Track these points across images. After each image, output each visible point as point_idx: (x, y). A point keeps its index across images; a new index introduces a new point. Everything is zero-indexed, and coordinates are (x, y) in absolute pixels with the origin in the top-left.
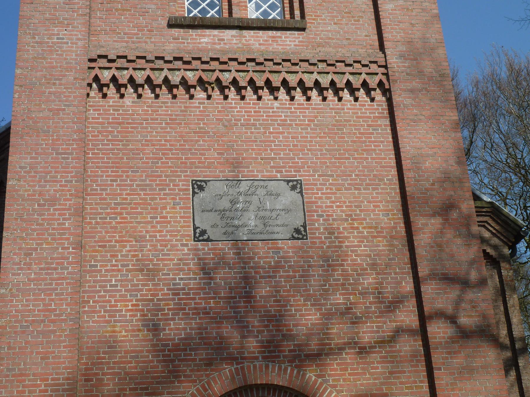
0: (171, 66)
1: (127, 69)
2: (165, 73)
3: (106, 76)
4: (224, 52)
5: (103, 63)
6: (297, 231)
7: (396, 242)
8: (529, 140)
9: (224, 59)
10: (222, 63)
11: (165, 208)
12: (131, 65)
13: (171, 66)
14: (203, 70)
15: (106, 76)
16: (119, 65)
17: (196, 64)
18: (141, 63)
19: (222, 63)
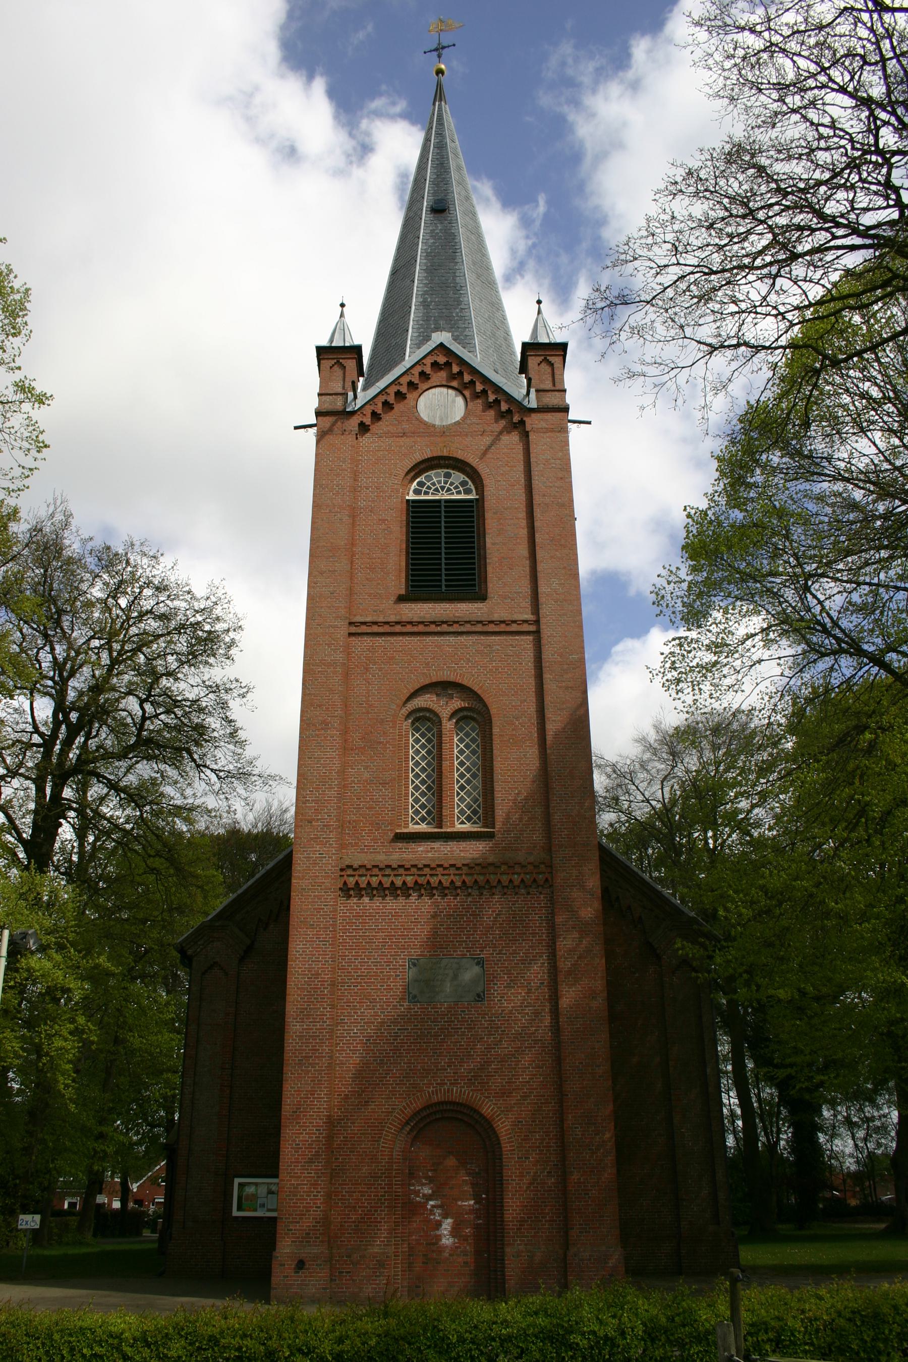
0: (396, 872)
1: (366, 875)
2: (391, 878)
3: (351, 881)
4: (433, 859)
5: (350, 872)
6: (478, 995)
7: (161, 996)
8: (904, 446)
9: (433, 865)
10: (432, 869)
11: (389, 979)
12: (369, 873)
13: (396, 872)
14: (419, 875)
15: (351, 881)
16: (361, 873)
17: (414, 870)
18: (376, 871)
19: (432, 869)
